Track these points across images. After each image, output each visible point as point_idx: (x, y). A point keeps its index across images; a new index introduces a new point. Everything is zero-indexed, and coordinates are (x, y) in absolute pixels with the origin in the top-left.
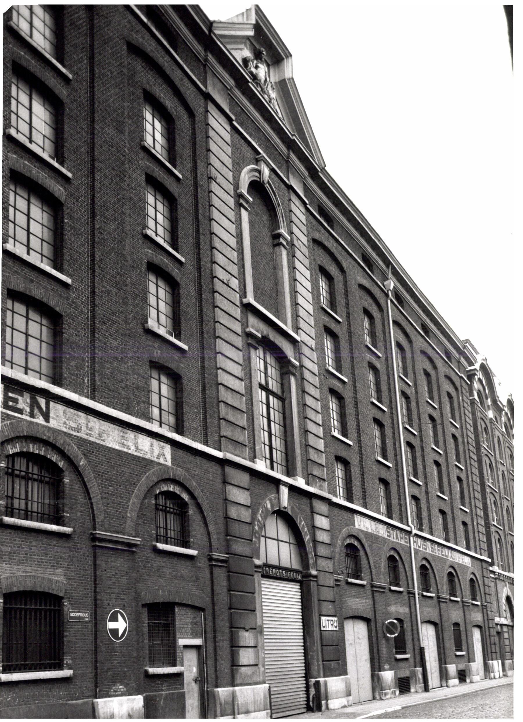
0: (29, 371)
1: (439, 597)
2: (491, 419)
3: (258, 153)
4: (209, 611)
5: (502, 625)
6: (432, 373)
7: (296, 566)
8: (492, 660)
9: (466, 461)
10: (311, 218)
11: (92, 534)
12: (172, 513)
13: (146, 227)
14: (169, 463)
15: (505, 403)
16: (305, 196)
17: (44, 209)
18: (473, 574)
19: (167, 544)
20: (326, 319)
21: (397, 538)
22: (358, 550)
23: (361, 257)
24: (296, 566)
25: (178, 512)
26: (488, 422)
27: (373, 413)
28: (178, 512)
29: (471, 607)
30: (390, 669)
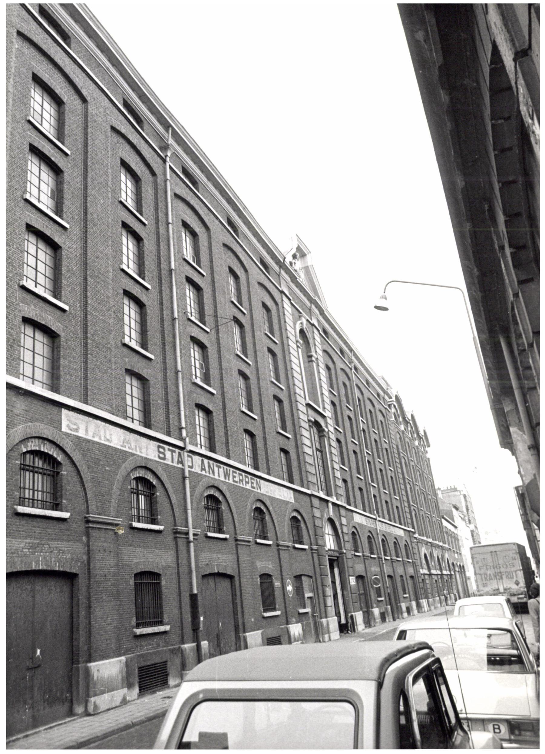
0: (35, 382)
1: (364, 556)
2: (403, 431)
3: (301, 313)
4: (314, 577)
5: (424, 574)
6: (347, 383)
7: (336, 549)
8: (422, 599)
9: (393, 465)
10: (322, 339)
11: (85, 517)
12: (40, 473)
13: (122, 262)
14: (293, 501)
15: (410, 418)
16: (290, 295)
17: (48, 252)
18: (406, 541)
19: (33, 507)
20: (235, 310)
21: (203, 469)
22: (264, 513)
23: (226, 221)
24: (336, 549)
25: (147, 494)
26: (401, 433)
27: (273, 391)
28: (147, 494)
29: (408, 564)
30: (297, 622)
